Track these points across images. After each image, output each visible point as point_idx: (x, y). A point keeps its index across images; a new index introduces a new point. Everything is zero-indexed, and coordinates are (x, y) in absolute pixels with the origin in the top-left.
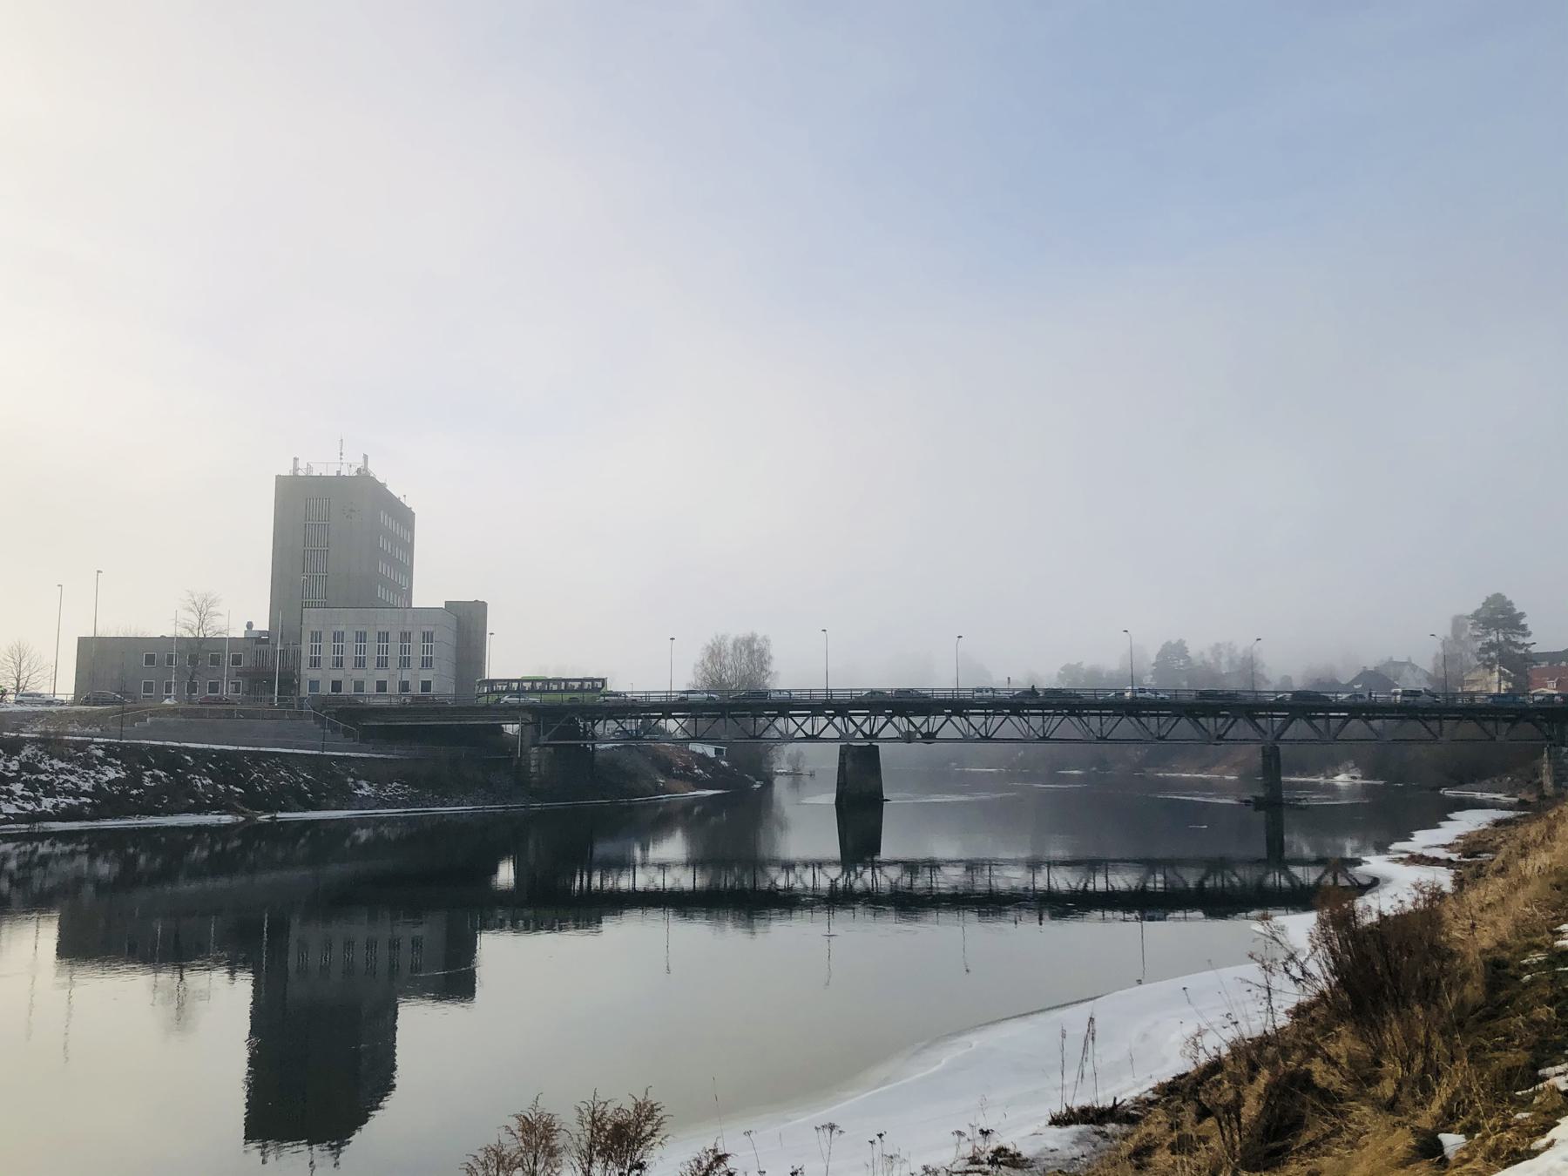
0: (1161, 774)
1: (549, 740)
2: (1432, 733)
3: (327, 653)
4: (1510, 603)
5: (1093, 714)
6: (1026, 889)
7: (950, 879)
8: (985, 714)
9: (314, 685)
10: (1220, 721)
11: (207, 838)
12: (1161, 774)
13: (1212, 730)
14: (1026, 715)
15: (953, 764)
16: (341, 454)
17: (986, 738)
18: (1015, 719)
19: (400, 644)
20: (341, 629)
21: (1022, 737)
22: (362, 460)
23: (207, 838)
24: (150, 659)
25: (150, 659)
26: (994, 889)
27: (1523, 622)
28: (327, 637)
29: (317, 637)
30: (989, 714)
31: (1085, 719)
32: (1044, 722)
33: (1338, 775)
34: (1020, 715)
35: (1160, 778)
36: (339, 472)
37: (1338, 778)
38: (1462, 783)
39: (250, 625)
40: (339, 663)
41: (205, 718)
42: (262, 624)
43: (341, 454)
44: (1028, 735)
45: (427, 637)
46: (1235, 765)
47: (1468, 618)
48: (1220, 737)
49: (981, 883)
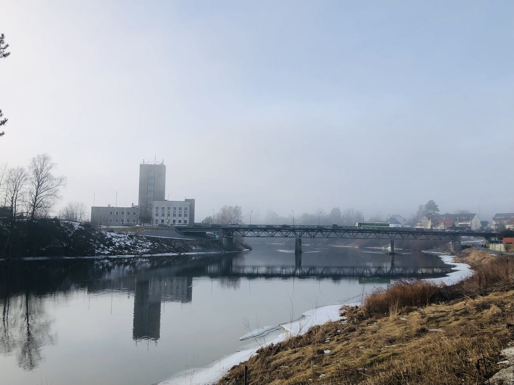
0: (334, 246)
1: (226, 236)
2: (390, 237)
3: (160, 212)
4: (435, 203)
5: (298, 231)
6: (252, 273)
7: (262, 270)
8: (258, 231)
9: (157, 221)
10: (314, 233)
11: (148, 264)
12: (334, 246)
13: (312, 235)
14: (268, 231)
15: (267, 242)
16: (155, 159)
17: (258, 236)
18: (251, 232)
19: (179, 210)
20: (164, 206)
21: (252, 236)
22: (162, 161)
23: (148, 264)
24: (111, 213)
25: (111, 213)
26: (239, 272)
27: (438, 208)
28: (160, 208)
29: (157, 208)
30: (259, 231)
31: (282, 232)
32: (286, 233)
33: (388, 247)
34: (267, 231)
35: (333, 247)
36: (155, 164)
37: (388, 248)
38: (427, 249)
39: (133, 204)
40: (163, 215)
41: (159, 230)
42: (136, 204)
43: (155, 159)
44: (254, 235)
45: (180, 209)
46: (357, 244)
47: (424, 206)
48: (314, 237)
49: (255, 272)
